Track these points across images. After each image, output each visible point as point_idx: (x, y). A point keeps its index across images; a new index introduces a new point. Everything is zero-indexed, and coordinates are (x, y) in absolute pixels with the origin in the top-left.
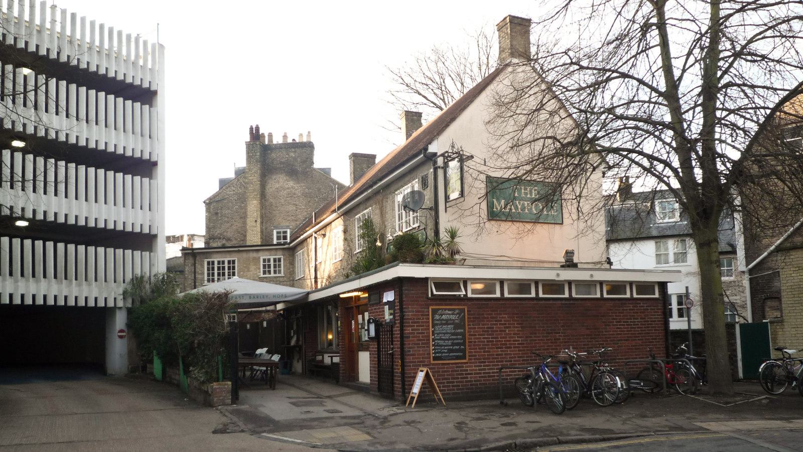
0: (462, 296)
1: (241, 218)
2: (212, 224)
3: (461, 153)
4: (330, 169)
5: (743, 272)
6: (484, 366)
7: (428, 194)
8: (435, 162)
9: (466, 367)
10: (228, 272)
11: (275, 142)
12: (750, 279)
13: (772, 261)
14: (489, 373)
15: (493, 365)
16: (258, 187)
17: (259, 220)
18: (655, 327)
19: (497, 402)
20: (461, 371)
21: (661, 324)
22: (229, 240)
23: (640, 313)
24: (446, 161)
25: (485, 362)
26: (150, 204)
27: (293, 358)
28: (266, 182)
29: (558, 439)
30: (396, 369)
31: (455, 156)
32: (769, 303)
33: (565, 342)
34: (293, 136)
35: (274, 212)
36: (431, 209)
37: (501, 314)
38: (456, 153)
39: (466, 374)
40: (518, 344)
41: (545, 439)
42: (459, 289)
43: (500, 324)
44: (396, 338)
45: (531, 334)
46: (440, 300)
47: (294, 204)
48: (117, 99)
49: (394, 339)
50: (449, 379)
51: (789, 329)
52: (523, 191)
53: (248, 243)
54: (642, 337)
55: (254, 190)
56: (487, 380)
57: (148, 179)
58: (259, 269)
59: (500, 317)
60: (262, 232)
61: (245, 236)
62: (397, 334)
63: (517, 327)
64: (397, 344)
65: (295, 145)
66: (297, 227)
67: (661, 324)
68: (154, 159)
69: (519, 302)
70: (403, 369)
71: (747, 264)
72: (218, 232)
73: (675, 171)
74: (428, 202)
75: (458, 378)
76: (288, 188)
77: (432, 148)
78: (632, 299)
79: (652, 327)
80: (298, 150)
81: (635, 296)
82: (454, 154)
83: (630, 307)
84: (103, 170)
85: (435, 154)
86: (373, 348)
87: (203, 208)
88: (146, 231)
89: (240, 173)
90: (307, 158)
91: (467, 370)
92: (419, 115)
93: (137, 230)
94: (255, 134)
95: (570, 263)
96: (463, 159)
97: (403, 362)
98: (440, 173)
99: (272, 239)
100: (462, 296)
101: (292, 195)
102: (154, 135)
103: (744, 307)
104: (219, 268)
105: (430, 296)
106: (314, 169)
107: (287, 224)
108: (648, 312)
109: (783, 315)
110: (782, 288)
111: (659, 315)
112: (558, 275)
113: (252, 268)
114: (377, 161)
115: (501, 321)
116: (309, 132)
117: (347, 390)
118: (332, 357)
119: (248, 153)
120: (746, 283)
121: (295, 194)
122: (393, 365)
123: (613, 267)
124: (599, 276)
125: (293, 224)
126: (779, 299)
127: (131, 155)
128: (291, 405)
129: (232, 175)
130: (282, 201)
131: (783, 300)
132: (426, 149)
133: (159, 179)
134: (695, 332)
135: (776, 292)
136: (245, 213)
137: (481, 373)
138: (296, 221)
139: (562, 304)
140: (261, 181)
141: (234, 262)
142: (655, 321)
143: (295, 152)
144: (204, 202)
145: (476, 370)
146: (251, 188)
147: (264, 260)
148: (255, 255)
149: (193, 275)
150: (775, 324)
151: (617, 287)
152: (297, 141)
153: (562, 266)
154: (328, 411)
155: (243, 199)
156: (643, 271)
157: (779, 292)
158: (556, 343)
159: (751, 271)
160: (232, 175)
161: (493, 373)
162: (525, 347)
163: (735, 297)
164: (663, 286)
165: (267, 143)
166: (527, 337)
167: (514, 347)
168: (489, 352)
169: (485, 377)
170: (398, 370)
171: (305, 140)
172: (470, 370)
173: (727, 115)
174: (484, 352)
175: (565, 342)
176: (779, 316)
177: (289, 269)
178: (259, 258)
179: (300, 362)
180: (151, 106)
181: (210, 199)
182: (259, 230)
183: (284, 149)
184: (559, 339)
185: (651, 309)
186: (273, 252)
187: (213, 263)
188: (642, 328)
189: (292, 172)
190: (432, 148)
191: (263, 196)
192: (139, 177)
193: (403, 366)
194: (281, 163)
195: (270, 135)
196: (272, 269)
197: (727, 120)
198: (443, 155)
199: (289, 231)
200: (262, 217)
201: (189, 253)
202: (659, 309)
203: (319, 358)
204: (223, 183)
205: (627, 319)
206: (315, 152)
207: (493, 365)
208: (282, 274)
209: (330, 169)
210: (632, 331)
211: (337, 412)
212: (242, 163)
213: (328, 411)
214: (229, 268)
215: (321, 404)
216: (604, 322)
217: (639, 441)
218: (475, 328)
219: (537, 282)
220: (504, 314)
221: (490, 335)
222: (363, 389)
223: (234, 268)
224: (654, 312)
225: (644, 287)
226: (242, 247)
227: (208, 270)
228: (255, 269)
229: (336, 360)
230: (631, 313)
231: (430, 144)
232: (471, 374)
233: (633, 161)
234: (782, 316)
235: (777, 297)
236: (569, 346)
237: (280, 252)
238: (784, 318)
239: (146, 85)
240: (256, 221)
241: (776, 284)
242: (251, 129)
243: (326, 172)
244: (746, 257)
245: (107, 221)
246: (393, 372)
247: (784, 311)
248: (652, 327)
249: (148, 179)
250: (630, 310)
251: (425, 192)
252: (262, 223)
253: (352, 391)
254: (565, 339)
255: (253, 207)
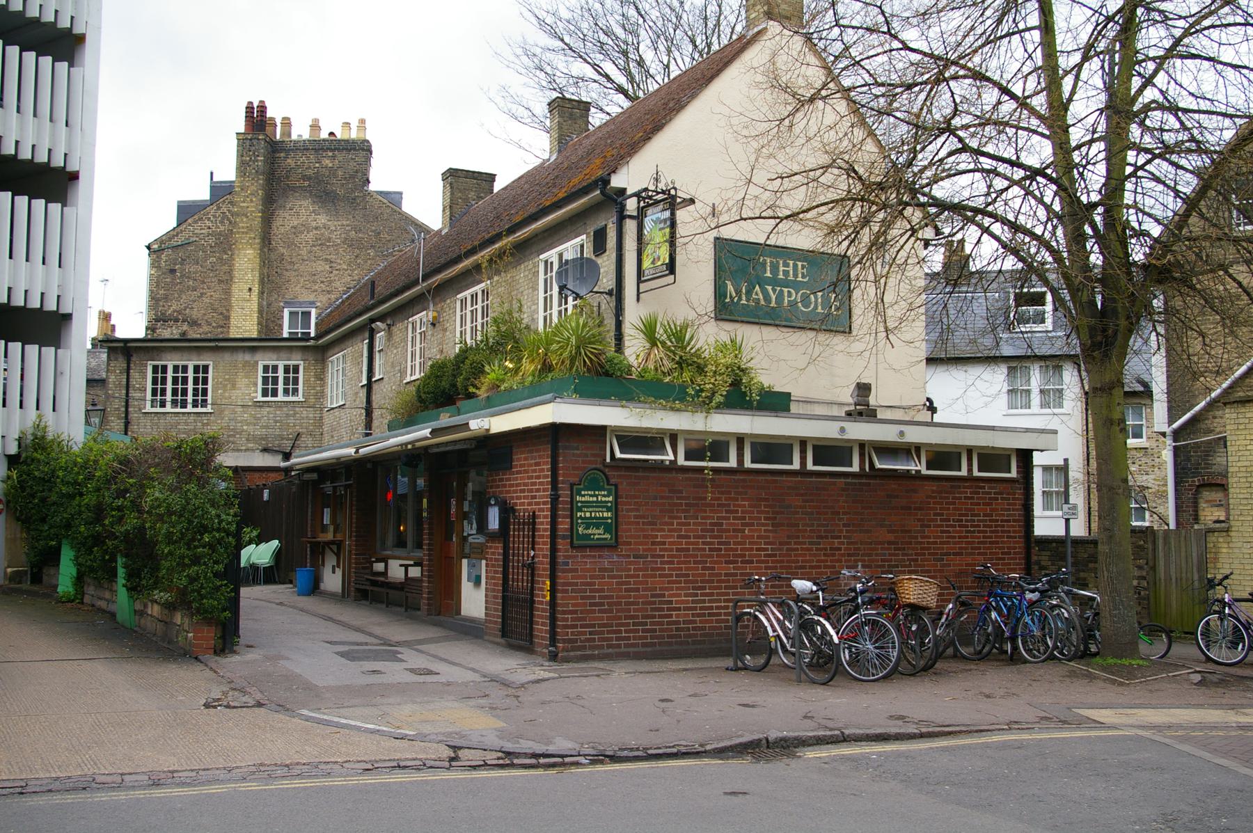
0: (667, 463)
1: (220, 281)
2: (162, 292)
3: (673, 192)
4: (401, 193)
5: (1164, 434)
6: (702, 595)
7: (606, 263)
8: (622, 207)
9: (670, 596)
10: (194, 389)
11: (294, 137)
12: (1175, 447)
13: (1215, 417)
14: (711, 608)
15: (718, 594)
16: (257, 223)
17: (256, 289)
18: (1009, 532)
19: (729, 662)
20: (661, 603)
21: (1019, 526)
22: (194, 323)
23: (984, 504)
24: (642, 204)
25: (704, 588)
26: (60, 254)
27: (323, 565)
28: (272, 214)
29: (843, 733)
30: (538, 596)
31: (660, 197)
32: (1207, 494)
33: (849, 555)
34: (331, 126)
35: (285, 272)
36: (610, 293)
37: (737, 500)
38: (663, 192)
39: (669, 609)
40: (766, 556)
41: (821, 733)
42: (662, 449)
43: (735, 518)
44: (542, 537)
45: (789, 537)
46: (628, 468)
47: (326, 260)
48: (40, 58)
49: (537, 540)
50: (637, 617)
51: (1239, 545)
52: (781, 269)
53: (233, 334)
54: (984, 548)
55: (250, 229)
56: (707, 622)
57: (60, 205)
58: (255, 385)
59: (734, 506)
60: (260, 312)
61: (228, 318)
62: (545, 530)
63: (763, 525)
64: (542, 549)
65: (335, 146)
66: (330, 305)
67: (1019, 526)
68: (72, 167)
69: (769, 478)
70: (553, 597)
71: (1171, 421)
72: (173, 307)
73: (1054, 253)
74: (607, 281)
75: (654, 617)
76: (316, 228)
77: (617, 181)
78: (970, 479)
79: (1002, 532)
80: (340, 156)
81: (976, 473)
82: (658, 193)
83: (966, 493)
84: (26, 197)
85: (622, 191)
86: (493, 553)
87: (144, 259)
88: (51, 306)
89: (220, 191)
90: (357, 172)
91: (671, 602)
92: (585, 107)
93: (35, 303)
94: (257, 118)
95: (863, 411)
96: (672, 202)
97: (553, 584)
98: (630, 227)
99: (281, 326)
100: (667, 463)
101: (322, 242)
102: (76, 119)
103: (1163, 495)
104: (175, 381)
105: (608, 460)
106: (370, 194)
107: (312, 298)
108: (996, 504)
109: (1231, 518)
110: (1231, 470)
111: (1017, 510)
112: (842, 430)
113: (242, 382)
114: (498, 186)
115: (737, 512)
116: (362, 121)
117: (432, 632)
118: (406, 567)
119: (240, 155)
120: (1167, 455)
121: (329, 240)
122: (532, 589)
123: (938, 418)
124: (914, 435)
125: (323, 300)
126: (1223, 487)
127: (30, 157)
128: (343, 660)
129: (204, 195)
130: (304, 252)
131: (1231, 490)
132: (606, 182)
133: (79, 206)
134: (1077, 542)
135: (1220, 474)
136: (230, 272)
137: (695, 608)
138: (329, 292)
139: (847, 484)
140: (263, 212)
141: (206, 369)
142: (1008, 521)
143: (334, 157)
144: (148, 247)
145: (687, 602)
146: (243, 223)
147: (266, 369)
148: (247, 357)
149: (124, 392)
150: (1216, 534)
151: (943, 457)
152: (339, 137)
153: (849, 414)
154: (412, 671)
155: (225, 244)
156: (992, 428)
157: (1225, 475)
158: (833, 555)
159: (1177, 435)
160: (204, 195)
161: (717, 608)
162: (777, 561)
163: (1145, 477)
164: (1025, 457)
165: (278, 137)
166: (781, 544)
167: (758, 562)
168: (713, 569)
169: (704, 615)
170: (543, 596)
171: (354, 135)
172: (677, 602)
173: (1149, 162)
174: (703, 569)
175: (849, 555)
176: (1222, 518)
177: (314, 388)
178: (257, 363)
179: (339, 572)
180: (71, 65)
181: (160, 240)
182: (255, 307)
183: (313, 152)
184: (840, 549)
185: (1002, 499)
186: (283, 355)
187: (165, 368)
188: (986, 532)
189: (324, 194)
190: (617, 181)
191: (266, 240)
192: (43, 201)
193: (553, 591)
194: (305, 178)
195: (287, 123)
196: (281, 387)
197: (1146, 171)
198: (637, 195)
199: (314, 312)
200: (262, 282)
201: (117, 347)
202: (1018, 499)
203: (379, 567)
204: (187, 211)
205: (961, 515)
206: (373, 161)
207: (718, 594)
208: (300, 398)
209: (401, 193)
210: (967, 537)
211: (430, 673)
212: (227, 172)
213: (412, 671)
214: (196, 381)
215: (394, 657)
216: (919, 520)
217: (983, 740)
218: (689, 524)
219: (803, 442)
220: (743, 499)
221: (715, 537)
222: (470, 631)
223: (205, 381)
224: (1008, 504)
225: (991, 458)
226: (222, 345)
227: (155, 381)
228: (247, 386)
229: (415, 572)
230: (967, 504)
231: (614, 172)
232: (679, 609)
233: (986, 230)
234: (1228, 519)
235: (1220, 485)
236: (856, 561)
237: (299, 355)
238: (1232, 523)
239: (64, 23)
240: (250, 289)
241: (1218, 459)
242: (250, 108)
243: (393, 199)
244: (1170, 409)
245: (12, 291)
246: (533, 602)
247: (1232, 512)
248: (1002, 532)
249: (60, 205)
250: (966, 498)
251: (599, 261)
252: (261, 293)
253: (452, 633)
254: (850, 549)
255: (246, 262)
